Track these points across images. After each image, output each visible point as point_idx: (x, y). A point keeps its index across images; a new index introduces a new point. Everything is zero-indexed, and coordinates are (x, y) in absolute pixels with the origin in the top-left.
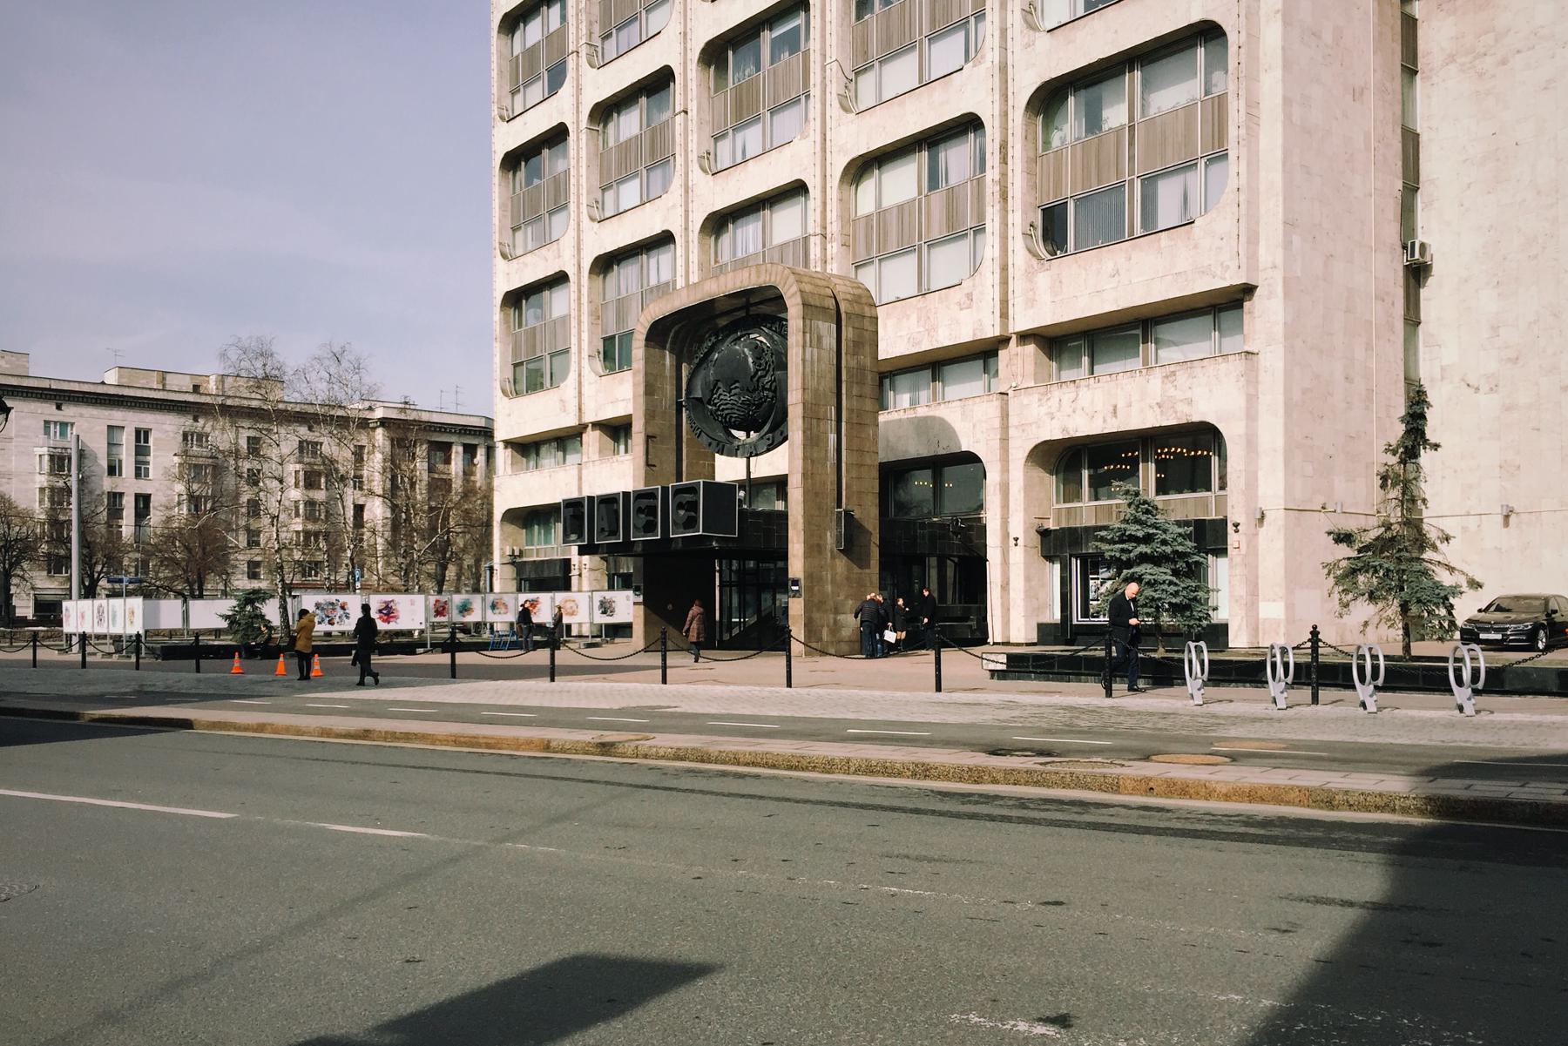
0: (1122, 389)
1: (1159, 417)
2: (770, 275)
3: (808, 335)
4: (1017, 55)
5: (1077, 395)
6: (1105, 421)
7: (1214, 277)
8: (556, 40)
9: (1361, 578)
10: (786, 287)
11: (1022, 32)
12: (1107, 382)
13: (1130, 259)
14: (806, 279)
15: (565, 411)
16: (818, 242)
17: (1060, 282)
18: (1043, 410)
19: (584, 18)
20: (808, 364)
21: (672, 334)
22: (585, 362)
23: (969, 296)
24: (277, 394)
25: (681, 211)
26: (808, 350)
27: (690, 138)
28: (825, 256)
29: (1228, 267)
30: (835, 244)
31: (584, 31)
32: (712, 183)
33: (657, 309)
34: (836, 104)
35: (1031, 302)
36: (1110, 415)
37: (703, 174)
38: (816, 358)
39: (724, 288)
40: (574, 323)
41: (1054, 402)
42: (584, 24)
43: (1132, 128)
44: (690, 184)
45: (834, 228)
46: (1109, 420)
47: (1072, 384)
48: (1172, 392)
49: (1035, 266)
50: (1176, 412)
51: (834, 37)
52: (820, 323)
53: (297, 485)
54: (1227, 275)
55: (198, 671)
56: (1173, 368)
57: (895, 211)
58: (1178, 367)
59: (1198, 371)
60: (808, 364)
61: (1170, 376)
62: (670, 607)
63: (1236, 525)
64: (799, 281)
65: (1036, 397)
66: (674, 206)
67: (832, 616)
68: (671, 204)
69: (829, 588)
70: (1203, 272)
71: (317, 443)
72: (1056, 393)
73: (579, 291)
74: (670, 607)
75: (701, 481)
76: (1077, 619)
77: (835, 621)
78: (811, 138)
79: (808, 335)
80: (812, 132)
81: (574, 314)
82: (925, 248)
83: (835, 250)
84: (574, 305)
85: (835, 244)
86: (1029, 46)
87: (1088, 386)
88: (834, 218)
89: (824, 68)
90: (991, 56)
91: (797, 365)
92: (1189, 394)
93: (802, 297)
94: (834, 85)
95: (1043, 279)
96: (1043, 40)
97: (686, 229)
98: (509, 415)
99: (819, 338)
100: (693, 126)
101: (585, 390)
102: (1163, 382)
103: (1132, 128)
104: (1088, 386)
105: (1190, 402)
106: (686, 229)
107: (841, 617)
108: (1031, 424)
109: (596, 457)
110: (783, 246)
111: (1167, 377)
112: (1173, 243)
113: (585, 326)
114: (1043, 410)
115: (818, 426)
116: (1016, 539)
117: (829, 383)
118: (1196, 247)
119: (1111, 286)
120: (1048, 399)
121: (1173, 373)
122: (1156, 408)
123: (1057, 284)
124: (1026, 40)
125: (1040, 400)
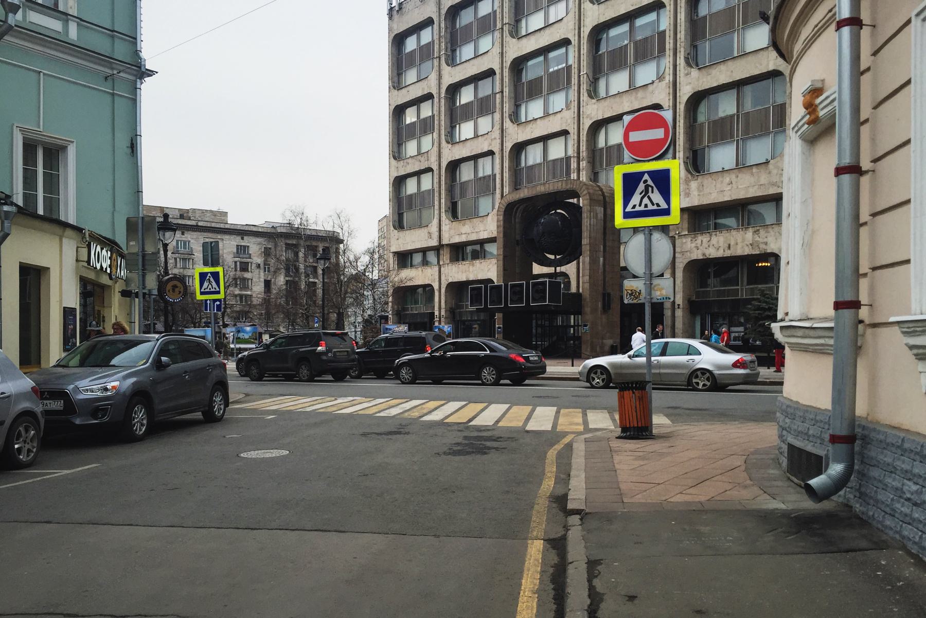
0: (733, 236)
1: (751, 250)
2: (573, 184)
3: (592, 213)
4: (681, 78)
5: (711, 239)
6: (724, 251)
7: (778, 187)
10: (581, 192)
11: (684, 68)
12: (725, 233)
13: (737, 177)
14: (590, 187)
15: (431, 238)
16: (576, 160)
17: (703, 186)
18: (693, 245)
19: (443, 40)
20: (592, 227)
21: (515, 209)
22: (443, 215)
25: (499, 141)
26: (592, 220)
27: (504, 105)
28: (579, 167)
30: (584, 162)
31: (443, 48)
32: (516, 128)
33: (511, 198)
34: (586, 94)
36: (727, 248)
37: (511, 124)
38: (595, 223)
39: (548, 190)
40: (436, 194)
41: (699, 241)
42: (444, 43)
43: (738, 116)
44: (504, 128)
45: (584, 153)
46: (726, 251)
47: (708, 234)
48: (757, 239)
49: (690, 178)
50: (759, 248)
51: (585, 62)
52: (597, 207)
55: (573, 366)
56: (758, 228)
58: (761, 228)
59: (770, 230)
60: (592, 227)
61: (757, 231)
62: (514, 336)
63: (679, 305)
64: (588, 189)
65: (690, 239)
66: (495, 139)
67: (601, 341)
68: (493, 137)
69: (600, 328)
70: (773, 185)
71: (245, 247)
72: (700, 238)
73: (440, 178)
74: (514, 336)
75: (547, 280)
77: (602, 343)
78: (572, 110)
79: (592, 213)
80: (572, 107)
81: (436, 189)
83: (584, 165)
84: (436, 186)
85: (584, 162)
86: (688, 74)
87: (716, 235)
88: (584, 149)
89: (579, 77)
91: (587, 227)
92: (765, 240)
93: (590, 197)
94: (585, 85)
97: (502, 150)
98: (398, 239)
99: (597, 214)
100: (506, 99)
102: (753, 234)
103: (738, 116)
104: (716, 235)
105: (766, 244)
106: (502, 150)
107: (604, 341)
108: (687, 252)
110: (554, 161)
111: (755, 232)
112: (758, 171)
113: (443, 196)
114: (693, 245)
115: (596, 254)
116: (679, 308)
117: (600, 236)
118: (770, 173)
119: (728, 189)
120: (696, 240)
121: (758, 230)
122: (750, 246)
123: (701, 187)
124: (686, 72)
125: (691, 240)
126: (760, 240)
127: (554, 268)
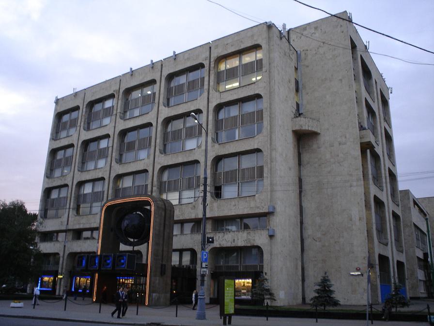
6: (231, 243)
8: (76, 120)
9: (18, 250)
23: (194, 206)
24: (287, 51)
25: (108, 172)
29: (264, 207)
35: (211, 210)
40: (69, 199)
48: (249, 237)
53: (203, 276)
54: (264, 209)
57: (230, 172)
76: (199, 297)
81: (69, 196)
82: (240, 184)
90: (265, 131)
95: (215, 205)
96: (217, 146)
101: (70, 219)
105: (254, 240)
109: (71, 240)
118: (256, 201)
126: (251, 238)
127: (132, 247)
